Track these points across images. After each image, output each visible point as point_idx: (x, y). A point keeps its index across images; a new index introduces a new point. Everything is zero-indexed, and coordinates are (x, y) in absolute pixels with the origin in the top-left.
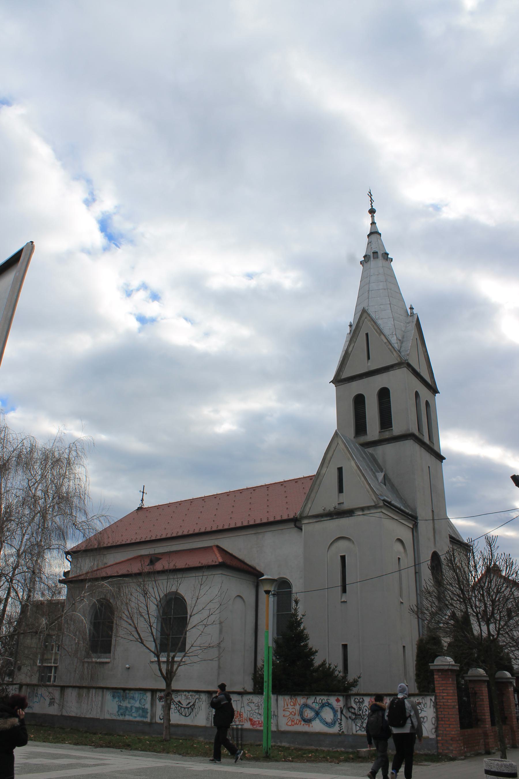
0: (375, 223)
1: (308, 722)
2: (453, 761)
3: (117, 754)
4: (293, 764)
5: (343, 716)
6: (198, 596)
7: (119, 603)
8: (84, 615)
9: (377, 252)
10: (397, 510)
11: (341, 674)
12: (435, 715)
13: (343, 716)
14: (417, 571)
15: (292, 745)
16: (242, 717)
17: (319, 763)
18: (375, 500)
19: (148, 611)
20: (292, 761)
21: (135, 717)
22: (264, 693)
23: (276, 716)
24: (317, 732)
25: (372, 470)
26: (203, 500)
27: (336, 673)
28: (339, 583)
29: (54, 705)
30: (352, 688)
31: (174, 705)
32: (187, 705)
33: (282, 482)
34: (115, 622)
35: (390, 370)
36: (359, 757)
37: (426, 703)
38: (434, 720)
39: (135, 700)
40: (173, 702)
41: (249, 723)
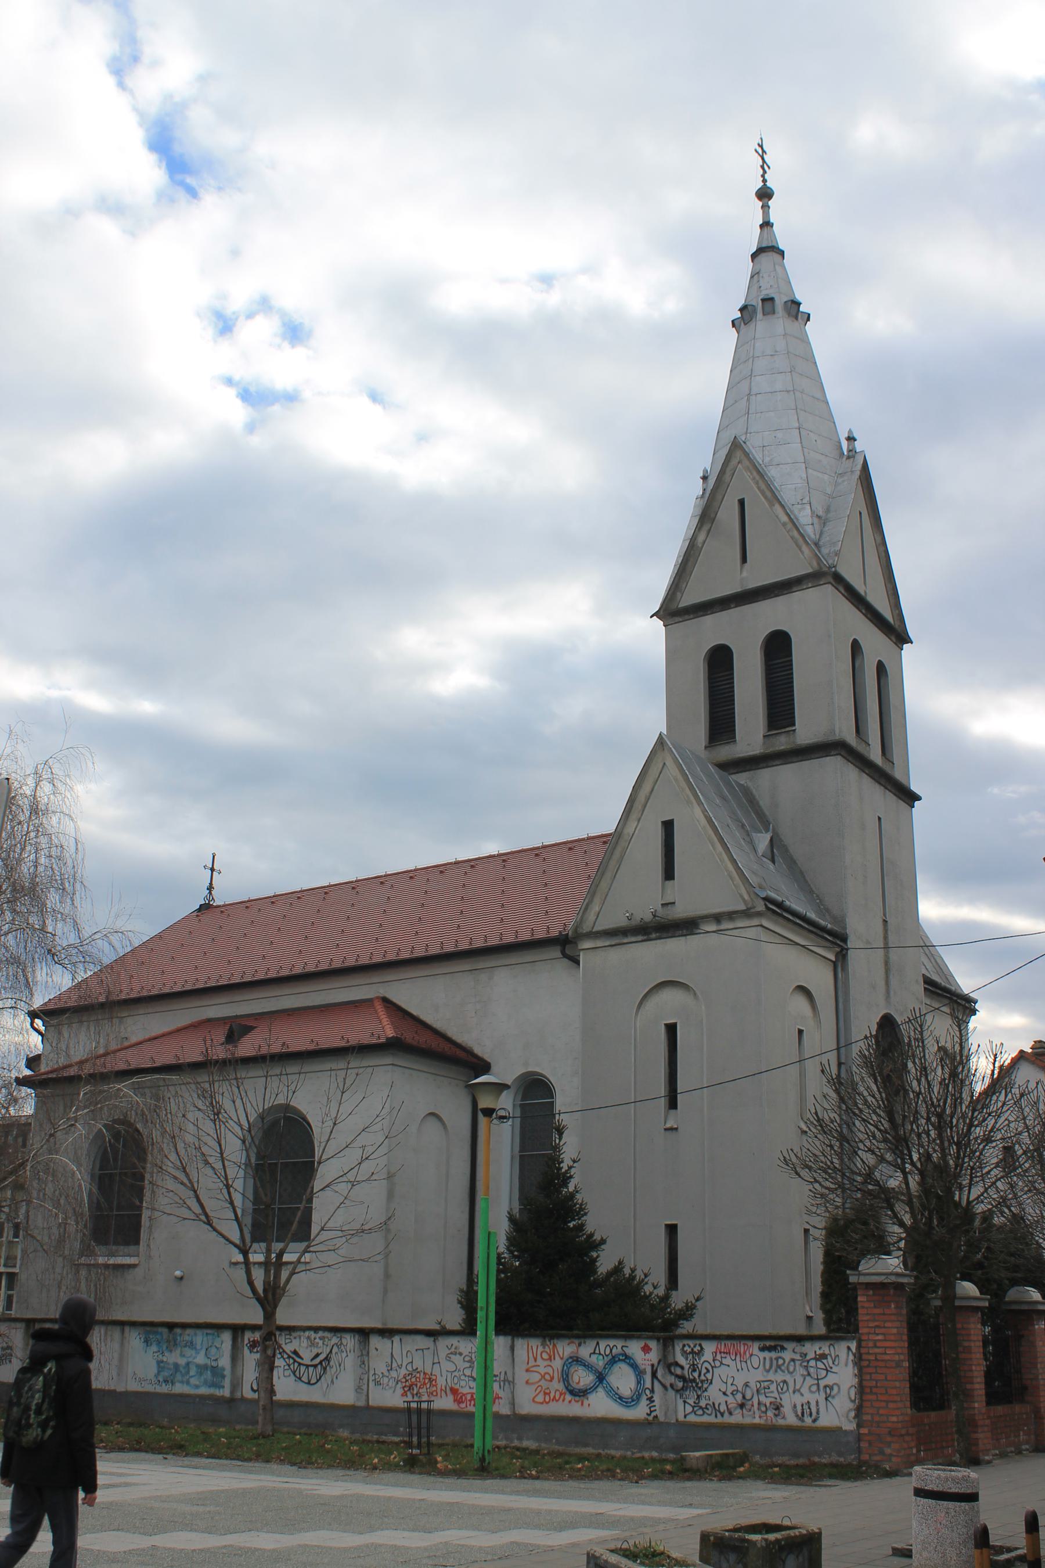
0: (772, 225)
1: (580, 1396)
2: (890, 1478)
3: (156, 1464)
4: (538, 1484)
5: (656, 1382)
6: (336, 1117)
7: (156, 1134)
8: (77, 1161)
9: (772, 299)
10: (798, 921)
11: (661, 1291)
12: (857, 1380)
13: (656, 1382)
14: (843, 1061)
15: (543, 1445)
16: (436, 1386)
17: (596, 1482)
18: (746, 897)
19: (222, 1154)
20: (537, 1478)
21: (197, 1387)
22: (478, 1333)
23: (509, 1382)
24: (598, 1419)
25: (743, 826)
26: (353, 888)
27: (648, 1289)
28: (662, 1089)
29: (10, 1361)
30: (681, 1322)
31: (284, 1359)
32: (312, 1360)
33: (538, 848)
34: (147, 1176)
35: (795, 589)
36: (686, 1470)
37: (838, 1356)
38: (853, 1392)
39: (195, 1348)
40: (280, 1353)
41: (451, 1398)
